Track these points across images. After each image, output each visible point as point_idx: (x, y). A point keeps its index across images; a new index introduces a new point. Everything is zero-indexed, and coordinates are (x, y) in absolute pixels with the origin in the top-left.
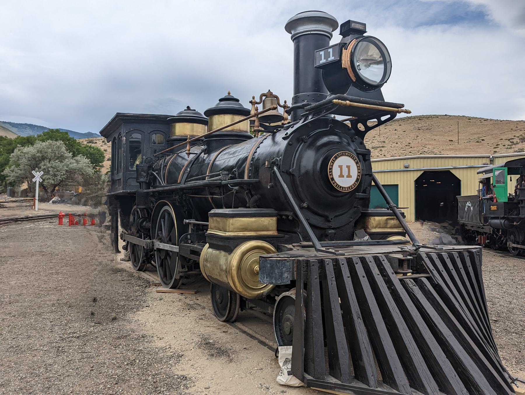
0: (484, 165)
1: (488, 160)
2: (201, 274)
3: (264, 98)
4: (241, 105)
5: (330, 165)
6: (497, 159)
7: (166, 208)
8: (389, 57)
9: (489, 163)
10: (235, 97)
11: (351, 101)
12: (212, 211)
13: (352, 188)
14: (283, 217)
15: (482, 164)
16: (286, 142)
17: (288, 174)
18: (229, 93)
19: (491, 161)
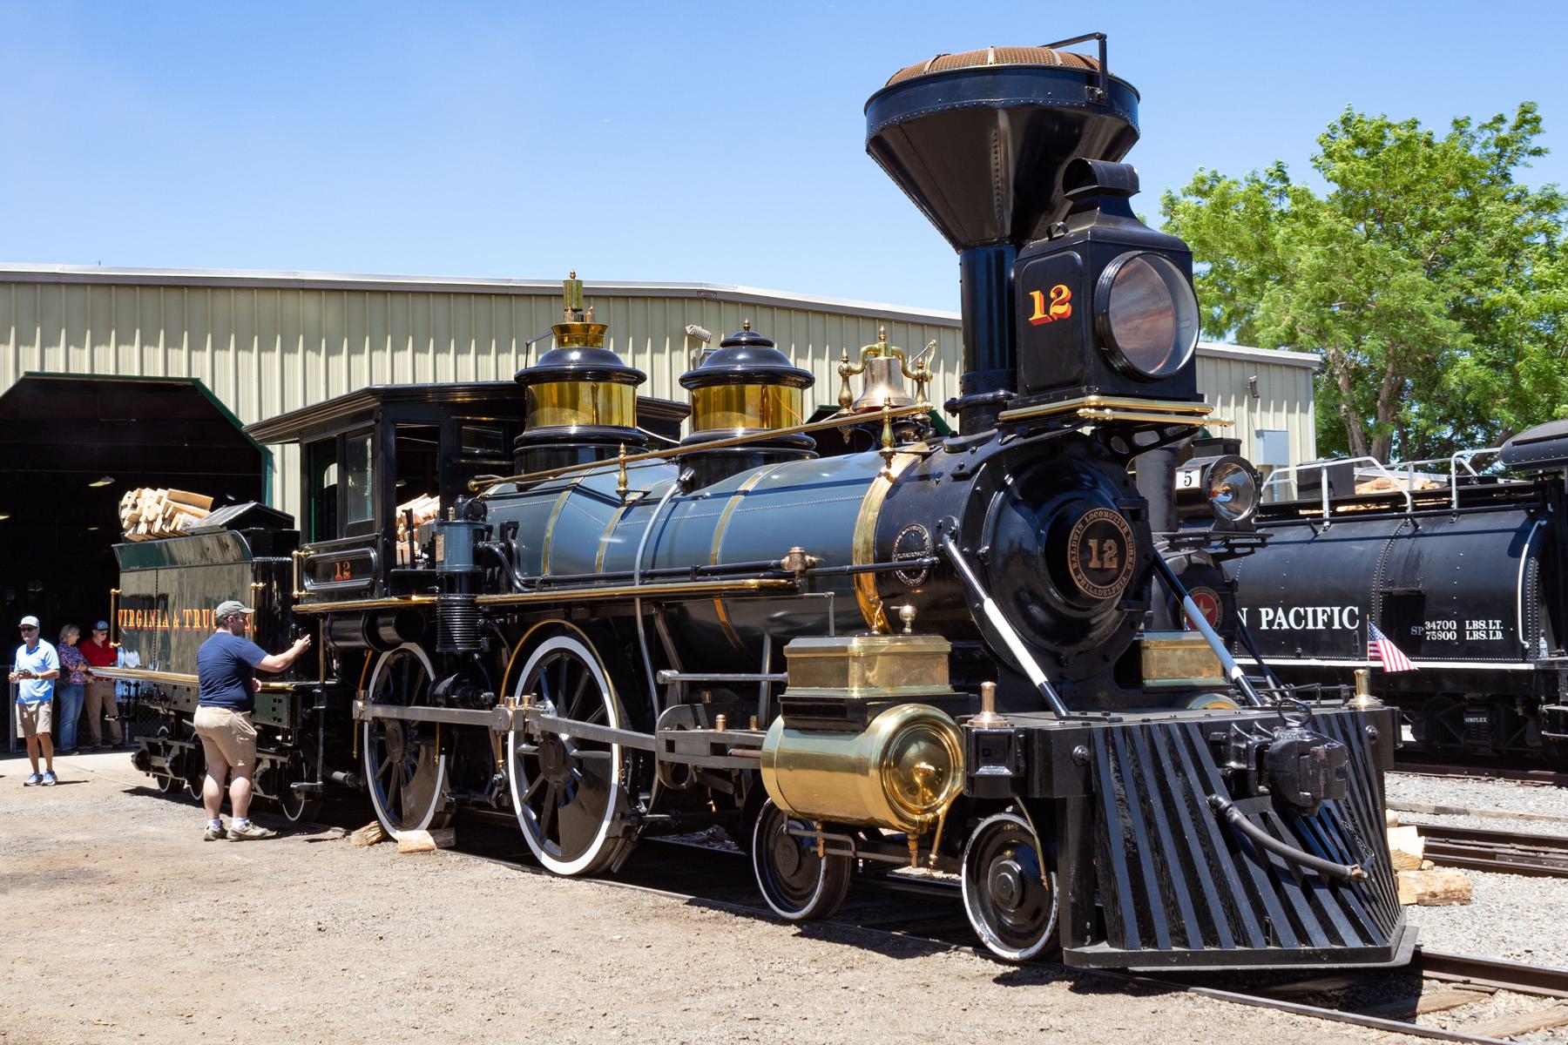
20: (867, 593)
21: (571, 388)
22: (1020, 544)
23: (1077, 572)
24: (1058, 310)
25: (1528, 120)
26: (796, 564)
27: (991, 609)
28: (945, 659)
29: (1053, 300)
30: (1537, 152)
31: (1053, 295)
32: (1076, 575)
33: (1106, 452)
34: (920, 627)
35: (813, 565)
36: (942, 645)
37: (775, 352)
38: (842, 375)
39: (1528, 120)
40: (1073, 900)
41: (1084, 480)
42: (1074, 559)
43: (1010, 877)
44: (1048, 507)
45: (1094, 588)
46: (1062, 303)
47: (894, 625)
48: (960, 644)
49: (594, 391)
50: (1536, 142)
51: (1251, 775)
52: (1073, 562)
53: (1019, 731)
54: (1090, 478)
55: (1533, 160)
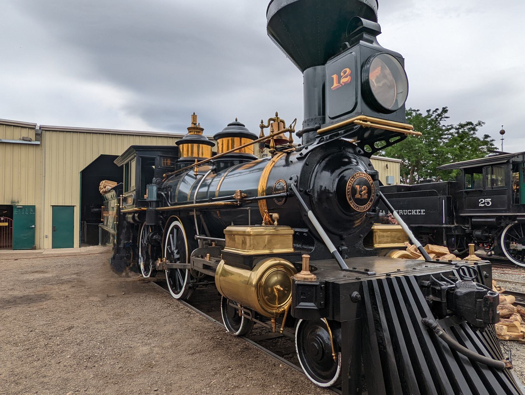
0: (23, 140)
1: (31, 134)
2: (214, 284)
3: (272, 122)
4: (246, 130)
5: (348, 186)
6: (48, 133)
7: (175, 223)
8: (405, 75)
9: (33, 138)
10: (242, 123)
11: (372, 122)
12: (228, 228)
13: (367, 208)
14: (304, 234)
15: (20, 139)
16: (301, 164)
17: (306, 194)
18: (236, 120)
19: (36, 134)
20: (263, 207)
21: (191, 146)
22: (325, 187)
23: (350, 199)
24: (344, 80)
25: (445, 110)
26: (238, 196)
27: (310, 214)
28: (291, 237)
29: (342, 76)
30: (447, 117)
31: (342, 74)
32: (350, 200)
33: (362, 152)
34: (281, 222)
35: (246, 197)
36: (289, 231)
37: (245, 128)
38: (261, 128)
39: (445, 110)
40: (349, 377)
41: (354, 162)
42: (348, 193)
43: (316, 345)
44: (338, 172)
45: (357, 207)
46: (346, 77)
47: (270, 223)
48: (297, 230)
49: (198, 147)
50: (446, 115)
51: (443, 305)
52: (348, 195)
53: (321, 283)
54: (356, 161)
55: (445, 119)
